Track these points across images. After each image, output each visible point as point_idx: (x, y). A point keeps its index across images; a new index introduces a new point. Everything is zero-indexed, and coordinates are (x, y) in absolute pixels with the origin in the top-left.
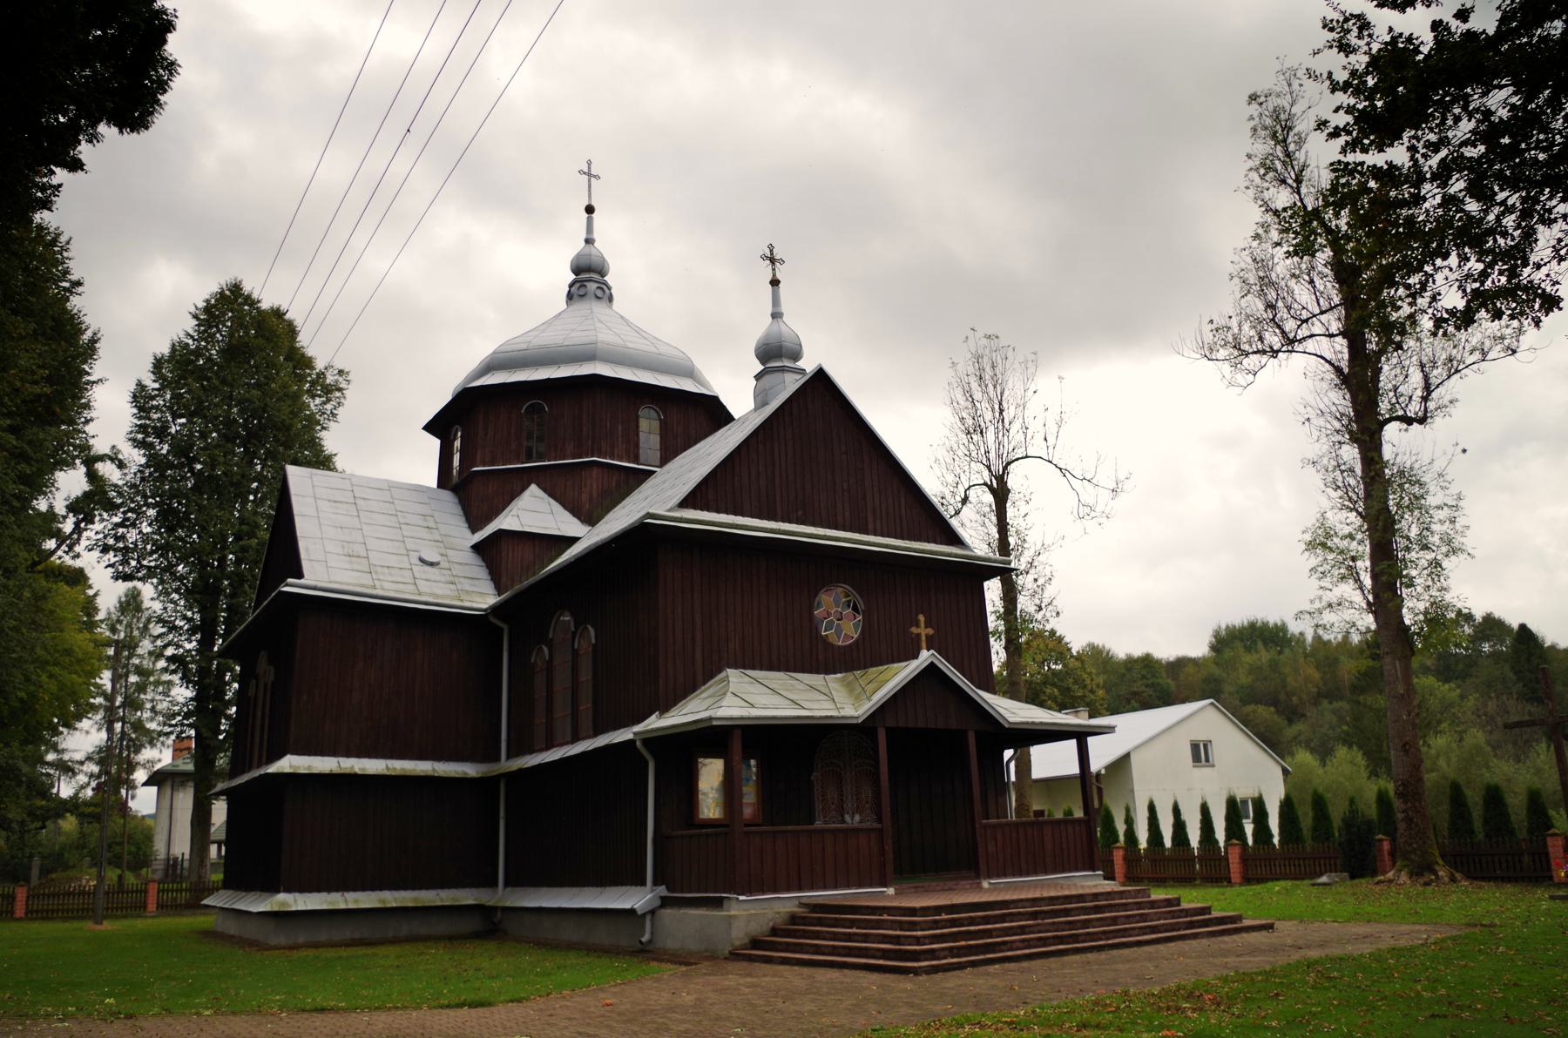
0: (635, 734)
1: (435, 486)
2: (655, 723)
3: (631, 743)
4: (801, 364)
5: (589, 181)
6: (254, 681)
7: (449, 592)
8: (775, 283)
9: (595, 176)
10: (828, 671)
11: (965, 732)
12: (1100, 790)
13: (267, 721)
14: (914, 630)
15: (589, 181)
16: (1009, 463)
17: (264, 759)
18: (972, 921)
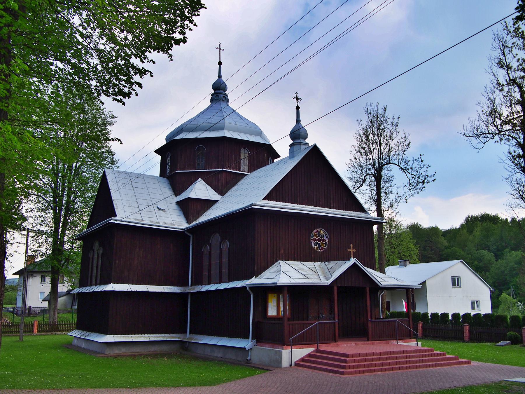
0: (247, 285)
1: (158, 175)
2: (254, 281)
3: (244, 288)
4: (307, 141)
5: (220, 52)
6: (92, 251)
7: (275, 304)
8: (298, 108)
9: (222, 49)
10: (315, 261)
11: (366, 288)
12: (413, 296)
13: (100, 267)
14: (349, 250)
15: (220, 52)
16: (382, 166)
17: (98, 282)
18: (327, 358)
